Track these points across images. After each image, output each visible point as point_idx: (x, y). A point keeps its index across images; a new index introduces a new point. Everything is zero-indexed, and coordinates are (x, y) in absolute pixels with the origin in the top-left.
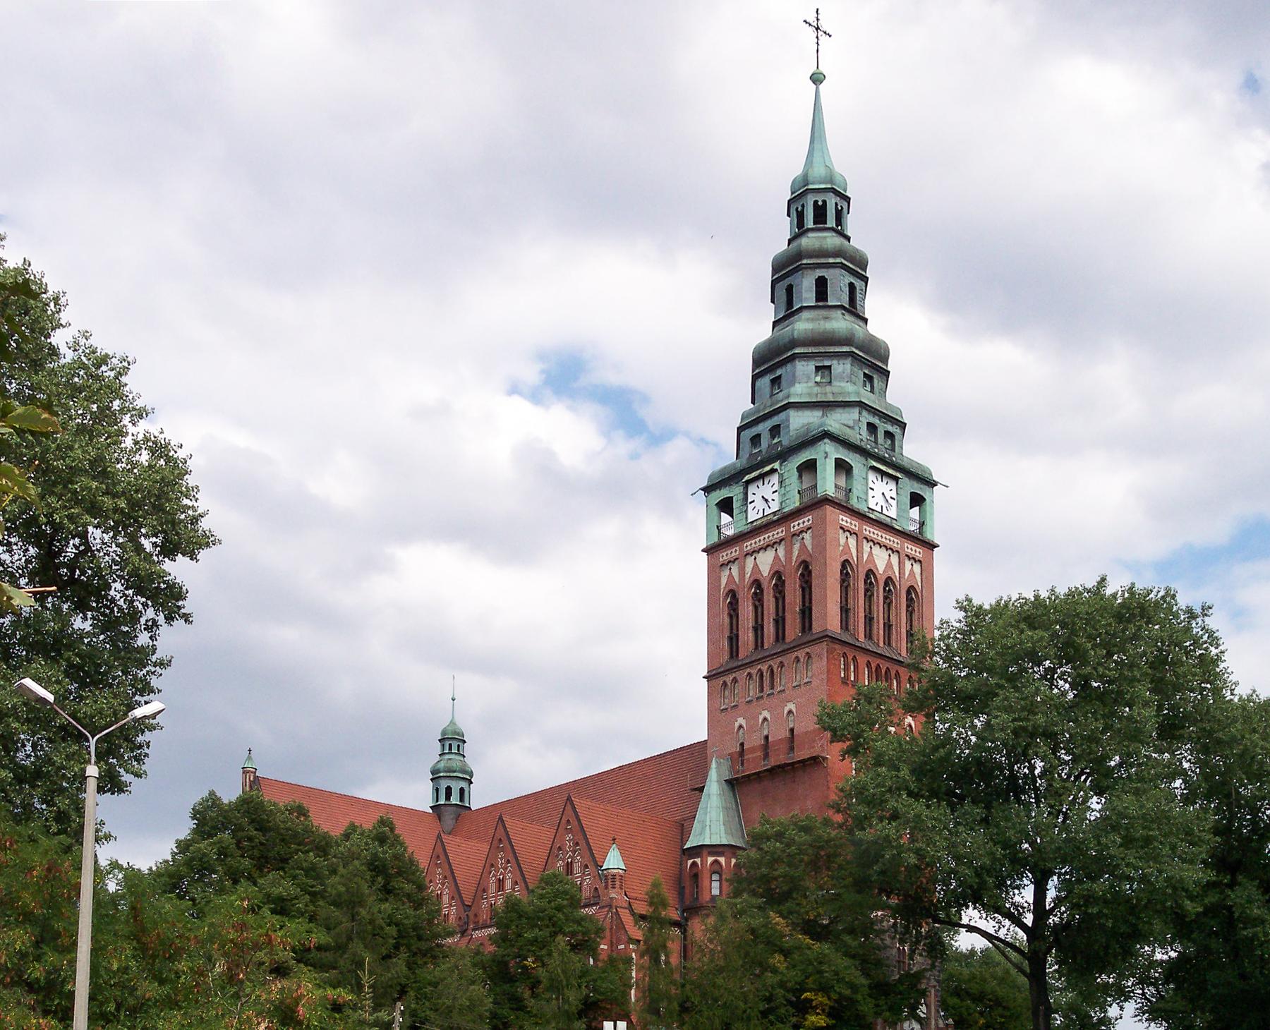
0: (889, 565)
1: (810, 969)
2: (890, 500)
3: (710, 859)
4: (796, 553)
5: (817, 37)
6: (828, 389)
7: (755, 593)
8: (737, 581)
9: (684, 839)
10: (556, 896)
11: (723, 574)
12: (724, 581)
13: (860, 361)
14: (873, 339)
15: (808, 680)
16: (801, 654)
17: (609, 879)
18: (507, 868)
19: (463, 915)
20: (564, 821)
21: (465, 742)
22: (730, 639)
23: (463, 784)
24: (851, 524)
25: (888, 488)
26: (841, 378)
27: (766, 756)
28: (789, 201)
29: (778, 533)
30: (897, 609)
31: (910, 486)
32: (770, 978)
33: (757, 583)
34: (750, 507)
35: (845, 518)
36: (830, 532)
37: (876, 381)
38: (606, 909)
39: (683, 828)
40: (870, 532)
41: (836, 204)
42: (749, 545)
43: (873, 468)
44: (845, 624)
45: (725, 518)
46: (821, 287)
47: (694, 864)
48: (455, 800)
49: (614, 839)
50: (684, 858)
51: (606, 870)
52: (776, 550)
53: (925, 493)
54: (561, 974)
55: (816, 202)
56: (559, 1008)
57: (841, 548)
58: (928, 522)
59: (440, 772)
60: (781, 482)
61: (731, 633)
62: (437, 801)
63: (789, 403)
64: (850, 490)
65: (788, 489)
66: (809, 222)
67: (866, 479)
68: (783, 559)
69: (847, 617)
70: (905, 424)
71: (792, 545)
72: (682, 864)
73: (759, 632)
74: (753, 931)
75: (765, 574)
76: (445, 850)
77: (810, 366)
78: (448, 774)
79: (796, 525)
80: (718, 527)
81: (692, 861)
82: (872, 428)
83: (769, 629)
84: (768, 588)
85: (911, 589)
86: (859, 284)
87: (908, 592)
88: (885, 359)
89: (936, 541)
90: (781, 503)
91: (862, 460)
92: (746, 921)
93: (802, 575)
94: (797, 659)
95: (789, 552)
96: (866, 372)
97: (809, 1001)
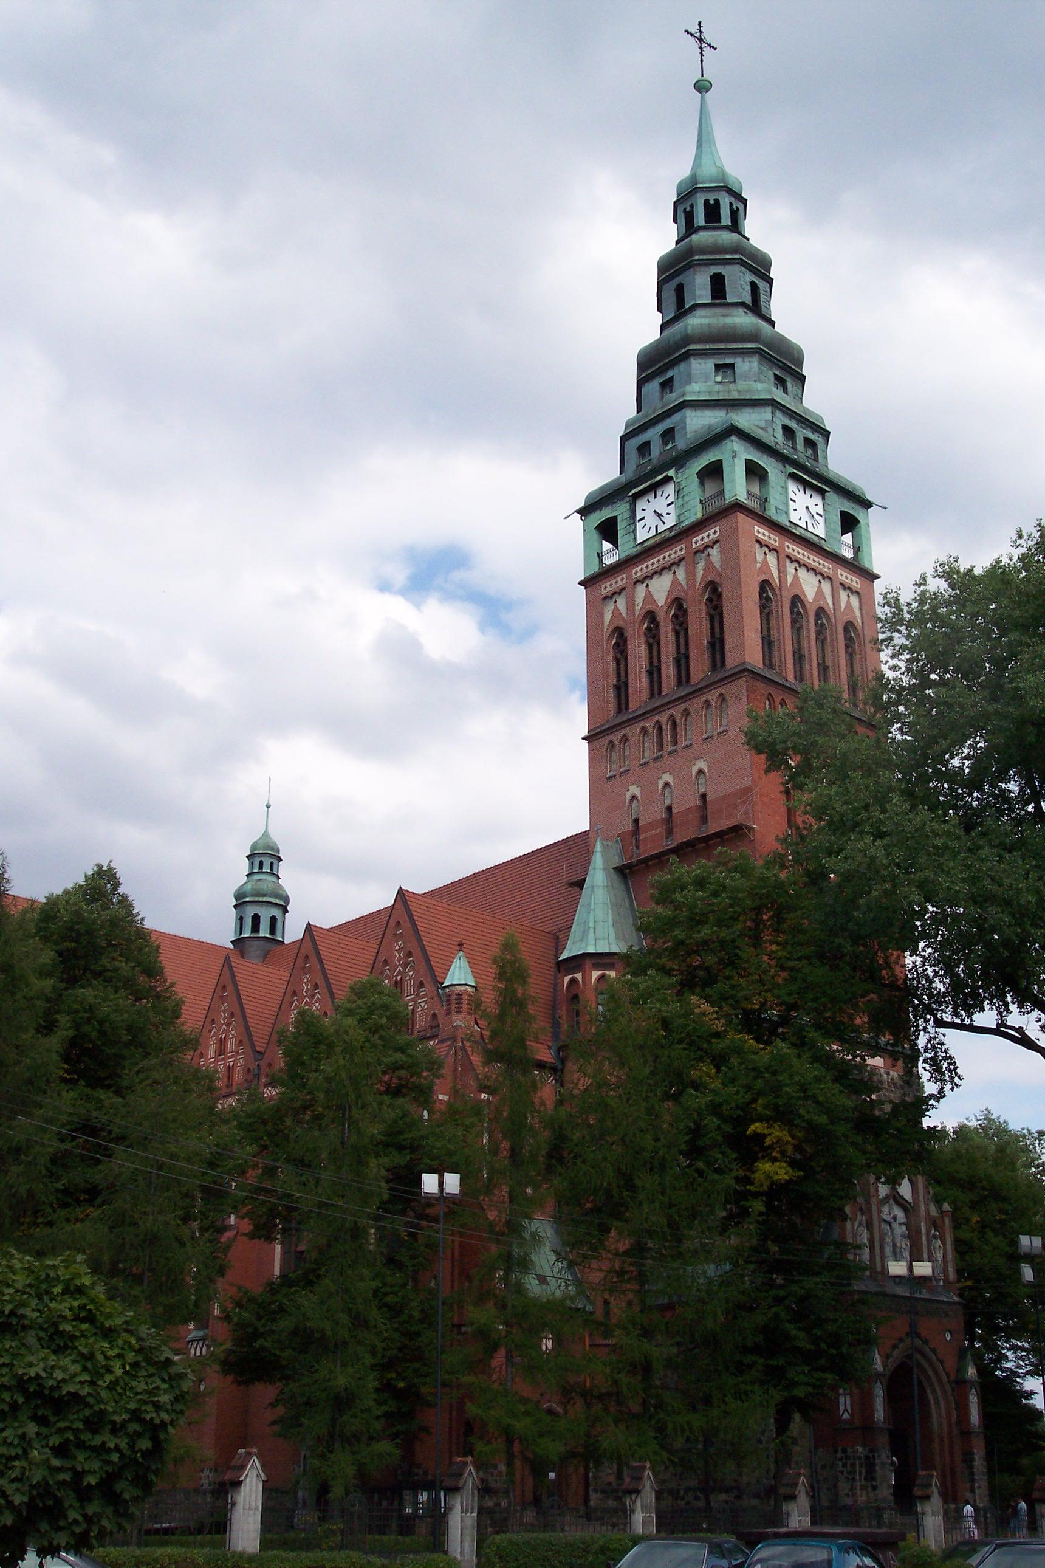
0: (820, 593)
1: (759, 1084)
2: (816, 516)
3: (596, 974)
4: (700, 573)
5: (701, 48)
6: (732, 386)
7: (649, 629)
8: (624, 614)
9: (559, 946)
10: (372, 1012)
11: (606, 609)
12: (608, 617)
13: (770, 360)
14: (782, 339)
15: (722, 729)
16: (712, 696)
17: (452, 999)
18: (313, 996)
19: (253, 1066)
20: (393, 923)
21: (280, 860)
22: (617, 688)
23: (276, 912)
24: (769, 538)
25: (814, 502)
26: (746, 377)
27: (669, 832)
28: (675, 203)
29: (676, 552)
30: (833, 655)
31: (840, 504)
32: (696, 1100)
33: (651, 616)
34: (639, 525)
35: (761, 531)
36: (745, 544)
37: (789, 385)
38: (449, 1043)
39: (558, 940)
40: (794, 550)
41: (731, 204)
42: (638, 571)
43: (793, 476)
44: (769, 662)
45: (607, 546)
46: (718, 285)
47: (573, 981)
48: (264, 932)
49: (461, 945)
50: (559, 975)
51: (448, 986)
52: (674, 572)
53: (858, 514)
54: (347, 1083)
55: (707, 202)
56: (343, 1143)
57: (759, 565)
58: (864, 548)
59: (246, 896)
60: (678, 492)
61: (619, 681)
62: (241, 934)
63: (684, 401)
64: (766, 499)
65: (686, 499)
66: (700, 220)
67: (785, 488)
68: (683, 583)
69: (770, 649)
70: (829, 432)
71: (695, 564)
72: (556, 984)
73: (655, 676)
74: (665, 1024)
75: (661, 603)
76: (233, 976)
77: (709, 365)
78: (256, 899)
79: (699, 540)
80: (598, 554)
81: (570, 977)
82: (788, 431)
83: (669, 670)
84: (665, 619)
85: (849, 625)
86: (761, 284)
87: (846, 629)
88: (800, 362)
89: (876, 571)
90: (679, 516)
91: (780, 466)
92: (653, 1006)
93: (710, 600)
94: (707, 704)
95: (691, 573)
96: (778, 373)
97: (759, 1137)
